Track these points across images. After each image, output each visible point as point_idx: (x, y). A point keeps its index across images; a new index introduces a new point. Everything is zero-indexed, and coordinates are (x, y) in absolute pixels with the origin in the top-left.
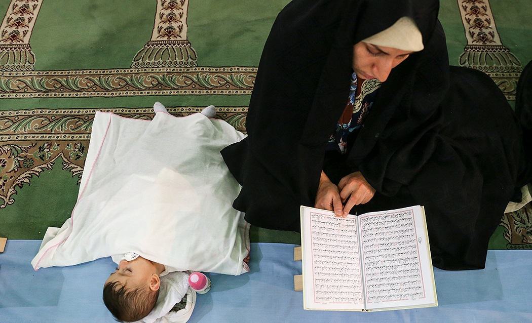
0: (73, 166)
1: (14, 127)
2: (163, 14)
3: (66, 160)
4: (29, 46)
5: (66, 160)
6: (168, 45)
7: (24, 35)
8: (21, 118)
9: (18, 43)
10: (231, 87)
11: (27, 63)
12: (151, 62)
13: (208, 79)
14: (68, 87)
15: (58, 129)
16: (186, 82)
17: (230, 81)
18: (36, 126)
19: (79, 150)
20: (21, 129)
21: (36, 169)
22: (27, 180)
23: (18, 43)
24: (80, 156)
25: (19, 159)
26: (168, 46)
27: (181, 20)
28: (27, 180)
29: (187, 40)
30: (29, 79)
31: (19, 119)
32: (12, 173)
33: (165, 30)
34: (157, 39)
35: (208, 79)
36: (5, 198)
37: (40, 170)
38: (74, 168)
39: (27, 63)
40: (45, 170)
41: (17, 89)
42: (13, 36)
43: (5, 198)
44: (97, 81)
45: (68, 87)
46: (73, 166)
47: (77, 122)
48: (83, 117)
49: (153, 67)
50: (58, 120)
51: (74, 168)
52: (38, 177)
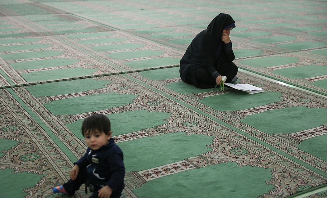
0: (275, 172)
28: (253, 166)
46: (275, 172)
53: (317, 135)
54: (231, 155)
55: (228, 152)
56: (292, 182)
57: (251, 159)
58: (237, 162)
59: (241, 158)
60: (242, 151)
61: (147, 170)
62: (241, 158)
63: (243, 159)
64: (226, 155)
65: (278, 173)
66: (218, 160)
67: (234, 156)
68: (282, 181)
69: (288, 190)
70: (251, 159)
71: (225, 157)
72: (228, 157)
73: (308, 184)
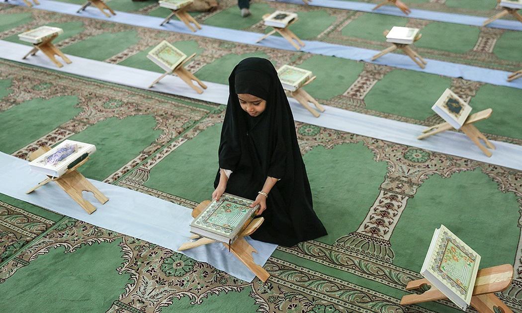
0: (126, 246)
1: (339, 293)
2: (373, 217)
3: (124, 241)
4: (389, 243)
5: (124, 241)
6: (370, 239)
7: (151, 164)
8: (315, 278)
9: (378, 237)
10: (357, 269)
11: (387, 256)
12: (351, 247)
13: (400, 277)
14: (302, 249)
15: (378, 309)
16: (379, 272)
17: (388, 275)
18: (358, 300)
19: (268, 288)
20: (285, 276)
21: (227, 287)
22: (90, 243)
23: (378, 237)
24: (267, 292)
25: (218, 275)
26: (369, 240)
27: (389, 227)
28: (90, 243)
29: (150, 170)
30: (387, 270)
31: (376, 300)
32: (209, 284)
33: (371, 228)
34: (518, 280)
35: (400, 277)
36: (197, 298)
37: (103, 241)
38: (126, 247)
39: (387, 256)
40: (234, 291)
41: (317, 255)
42: (374, 231)
43: (197, 298)
44: (356, 262)
45: (359, 267)
46: (126, 246)
47: (303, 277)
48: (309, 276)
49: (371, 257)
50: (348, 290)
51: (126, 247)
52: (227, 293)
53: (160, 160)
54: (107, 110)
55: (100, 108)
56: (177, 121)
57: (83, 230)
58: (63, 244)
59: (68, 234)
60: (116, 104)
61: (20, 150)
62: (68, 234)
63: (73, 235)
64: (100, 111)
65: (130, 245)
66: (32, 251)
67: (110, 110)
68: (167, 122)
69: (151, 274)
70: (83, 230)
71: (101, 114)
72: (104, 113)
73: (191, 119)
